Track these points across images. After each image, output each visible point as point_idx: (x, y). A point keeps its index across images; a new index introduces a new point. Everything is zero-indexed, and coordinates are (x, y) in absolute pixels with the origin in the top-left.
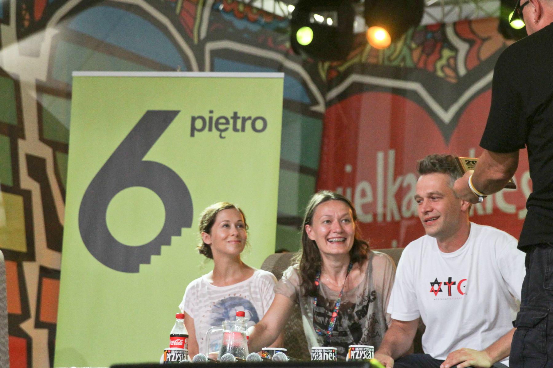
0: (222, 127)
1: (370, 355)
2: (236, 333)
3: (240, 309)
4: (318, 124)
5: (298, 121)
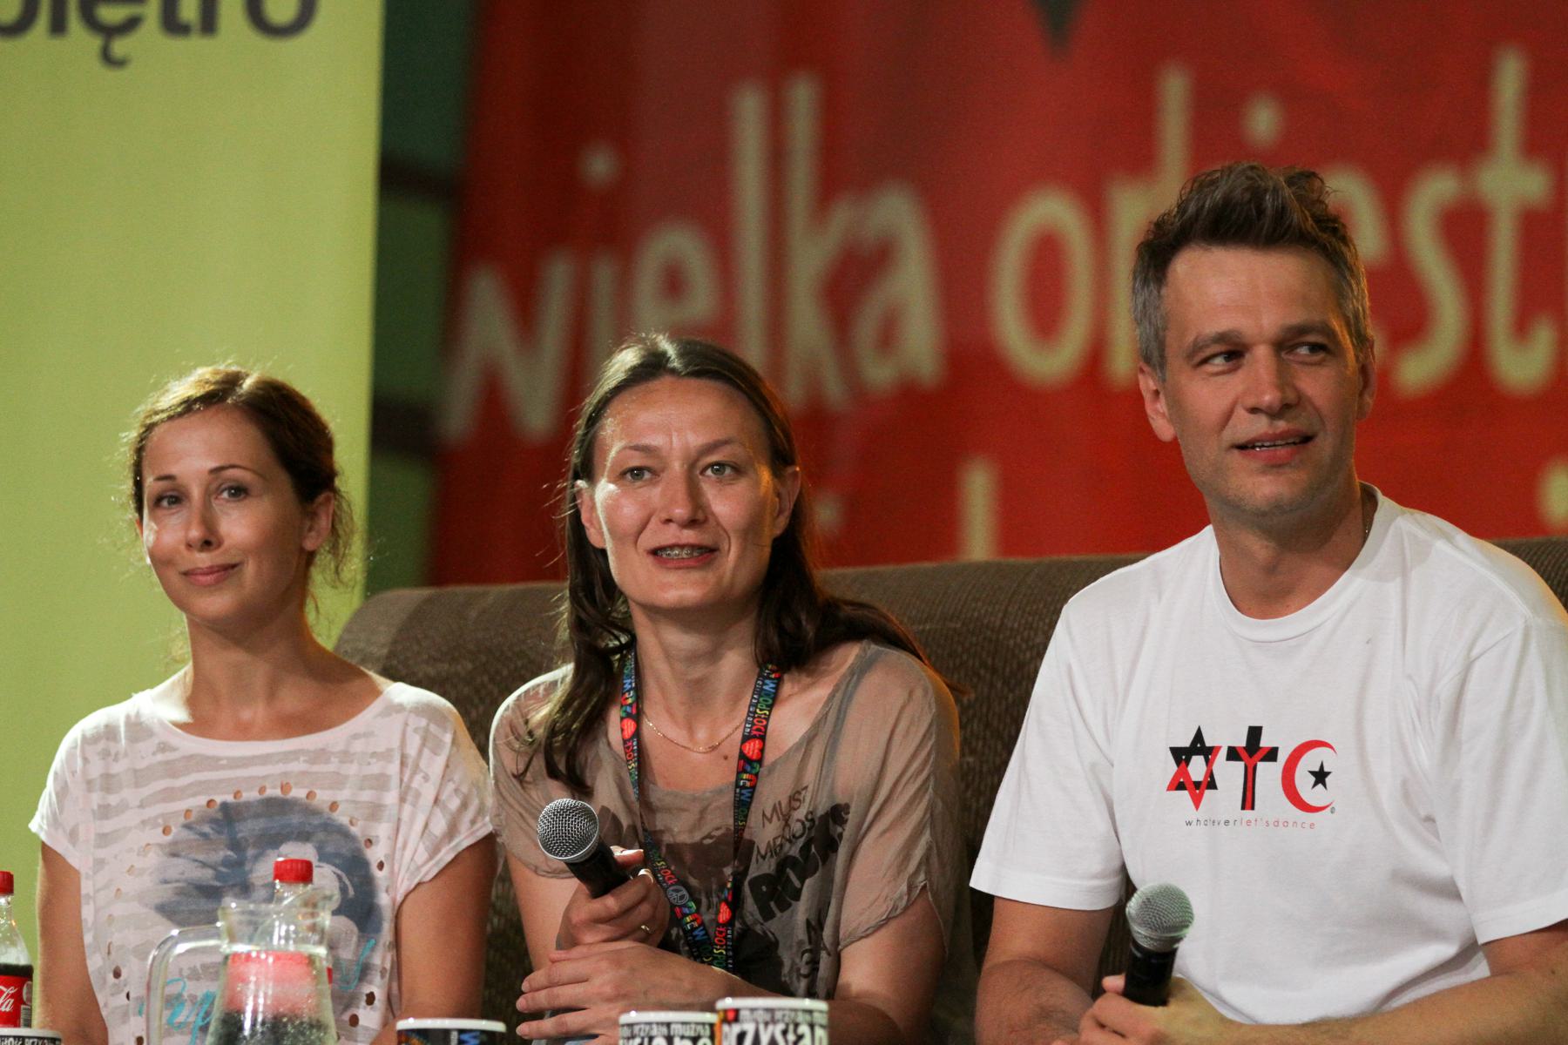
3: (295, 851)
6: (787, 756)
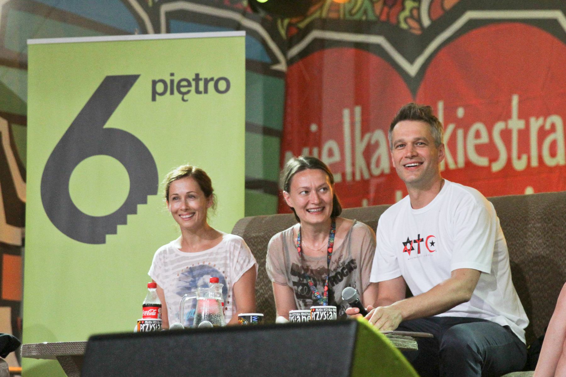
0: (184, 90)
1: (332, 315)
2: (210, 300)
4: (280, 83)
5: (260, 79)
6: (338, 249)
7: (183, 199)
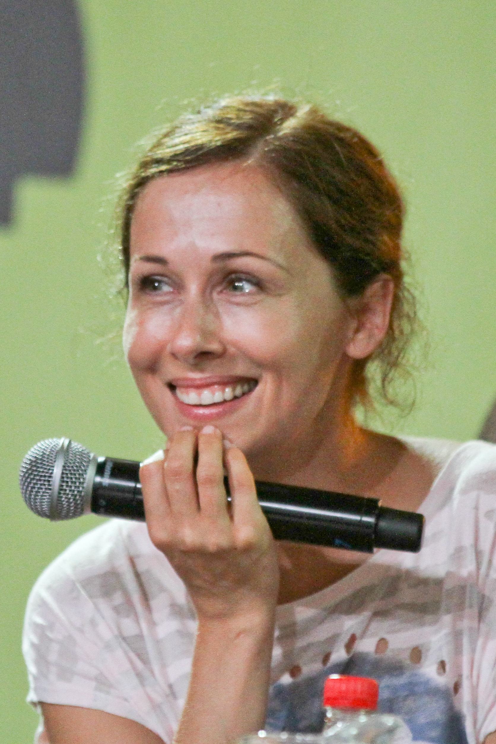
7: (193, 288)
